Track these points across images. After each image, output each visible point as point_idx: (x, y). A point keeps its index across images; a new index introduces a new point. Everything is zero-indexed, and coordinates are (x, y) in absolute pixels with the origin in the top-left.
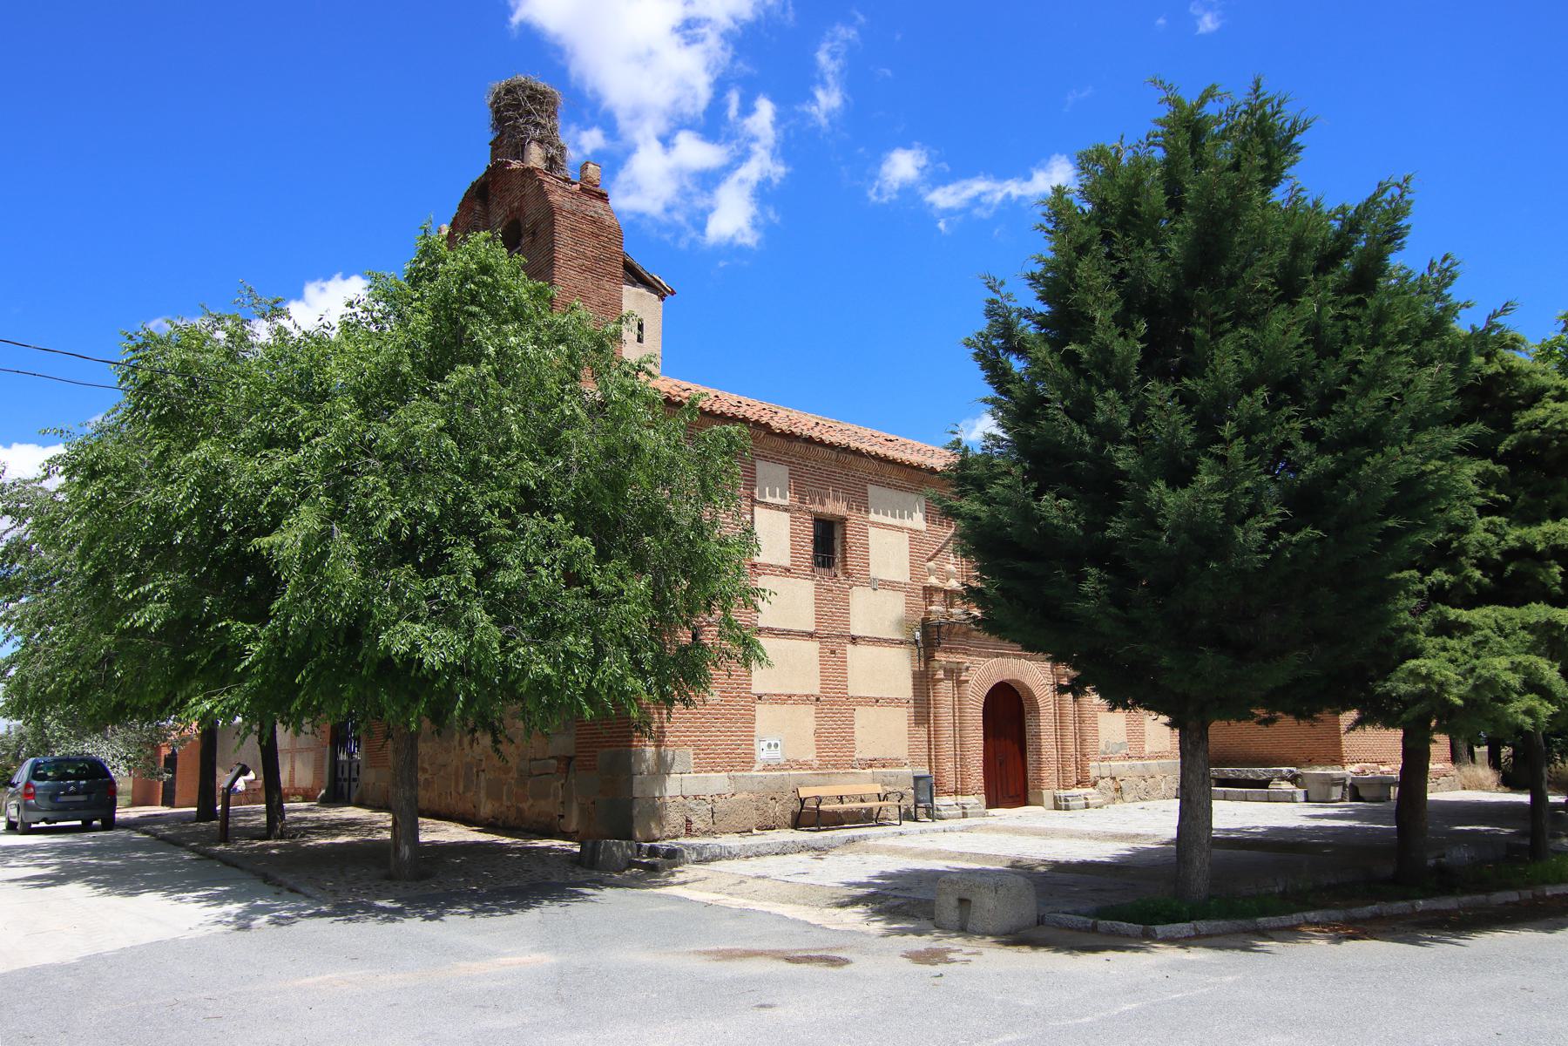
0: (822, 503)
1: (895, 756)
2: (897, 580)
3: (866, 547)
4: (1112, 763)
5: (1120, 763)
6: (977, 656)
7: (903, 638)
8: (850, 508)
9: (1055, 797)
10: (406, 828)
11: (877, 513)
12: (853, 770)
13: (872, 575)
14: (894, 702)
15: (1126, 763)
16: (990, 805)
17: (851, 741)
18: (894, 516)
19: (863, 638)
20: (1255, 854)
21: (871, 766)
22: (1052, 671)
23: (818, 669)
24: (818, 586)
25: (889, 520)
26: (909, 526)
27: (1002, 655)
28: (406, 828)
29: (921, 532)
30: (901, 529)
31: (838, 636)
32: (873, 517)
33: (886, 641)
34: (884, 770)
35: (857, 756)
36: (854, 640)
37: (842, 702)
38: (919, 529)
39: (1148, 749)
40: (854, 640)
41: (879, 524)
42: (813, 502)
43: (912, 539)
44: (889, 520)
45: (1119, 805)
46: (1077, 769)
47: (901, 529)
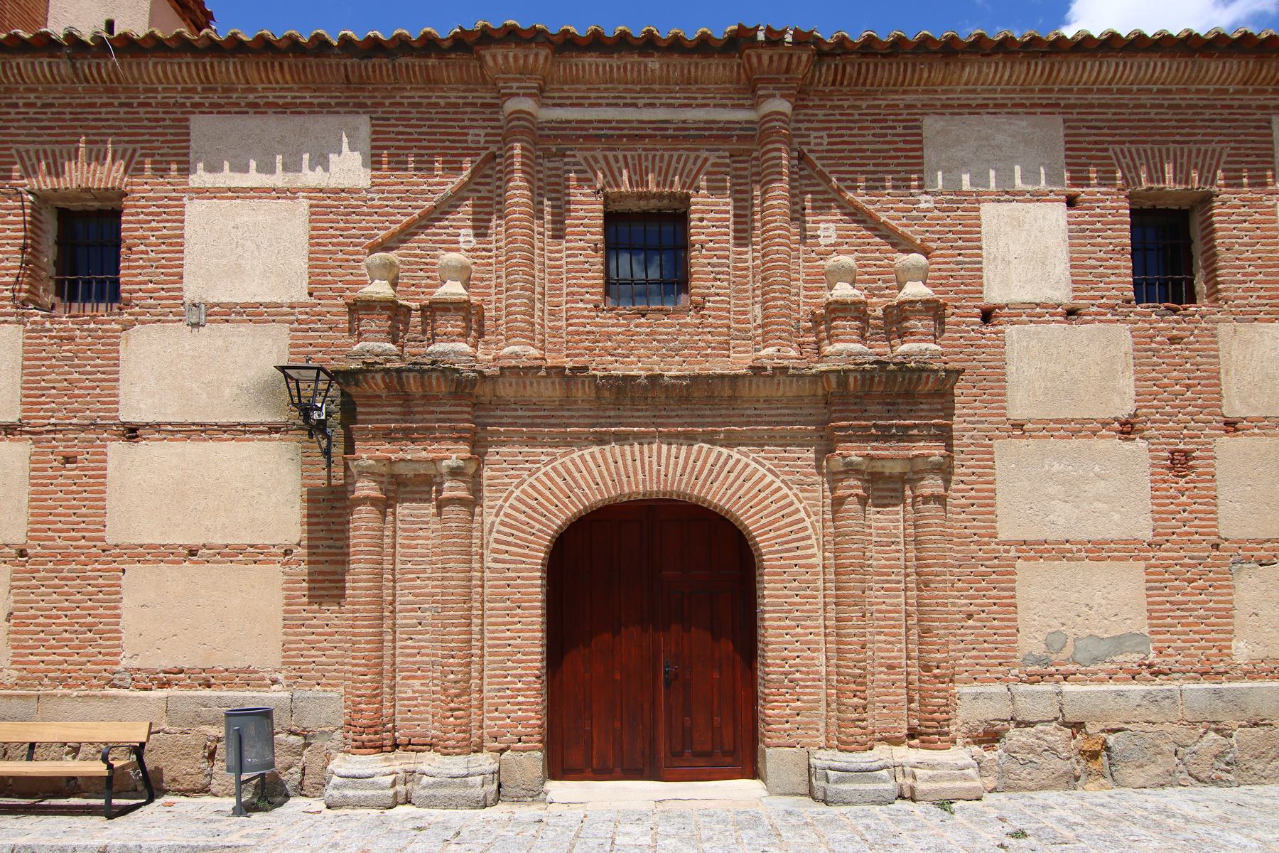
0: (56, 171)
1: (239, 665)
2: (267, 300)
3: (176, 244)
4: (1067, 687)
5: (1111, 687)
6: (521, 444)
7: (280, 419)
8: (134, 169)
9: (809, 766)
10: (109, 802)
11: (212, 168)
12: (114, 691)
13: (188, 296)
14: (256, 554)
15: (1136, 688)
16: (559, 768)
17: (114, 633)
18: (266, 168)
19: (157, 427)
20: (1164, 69)
21: (163, 685)
22: (818, 467)
23: (23, 495)
24: (31, 334)
25: (253, 179)
26: (313, 184)
27: (621, 438)
28: (109, 802)
29: (357, 191)
30: (289, 193)
31: (83, 428)
32: (200, 178)
33: (225, 428)
34: (206, 692)
35: (124, 662)
36: (132, 433)
37: (88, 555)
38: (347, 184)
39: (1242, 650)
40: (132, 433)
41: (219, 190)
42: (29, 172)
43: (316, 212)
44: (253, 179)
45: (1095, 794)
46: (910, 700)
47: (289, 193)
